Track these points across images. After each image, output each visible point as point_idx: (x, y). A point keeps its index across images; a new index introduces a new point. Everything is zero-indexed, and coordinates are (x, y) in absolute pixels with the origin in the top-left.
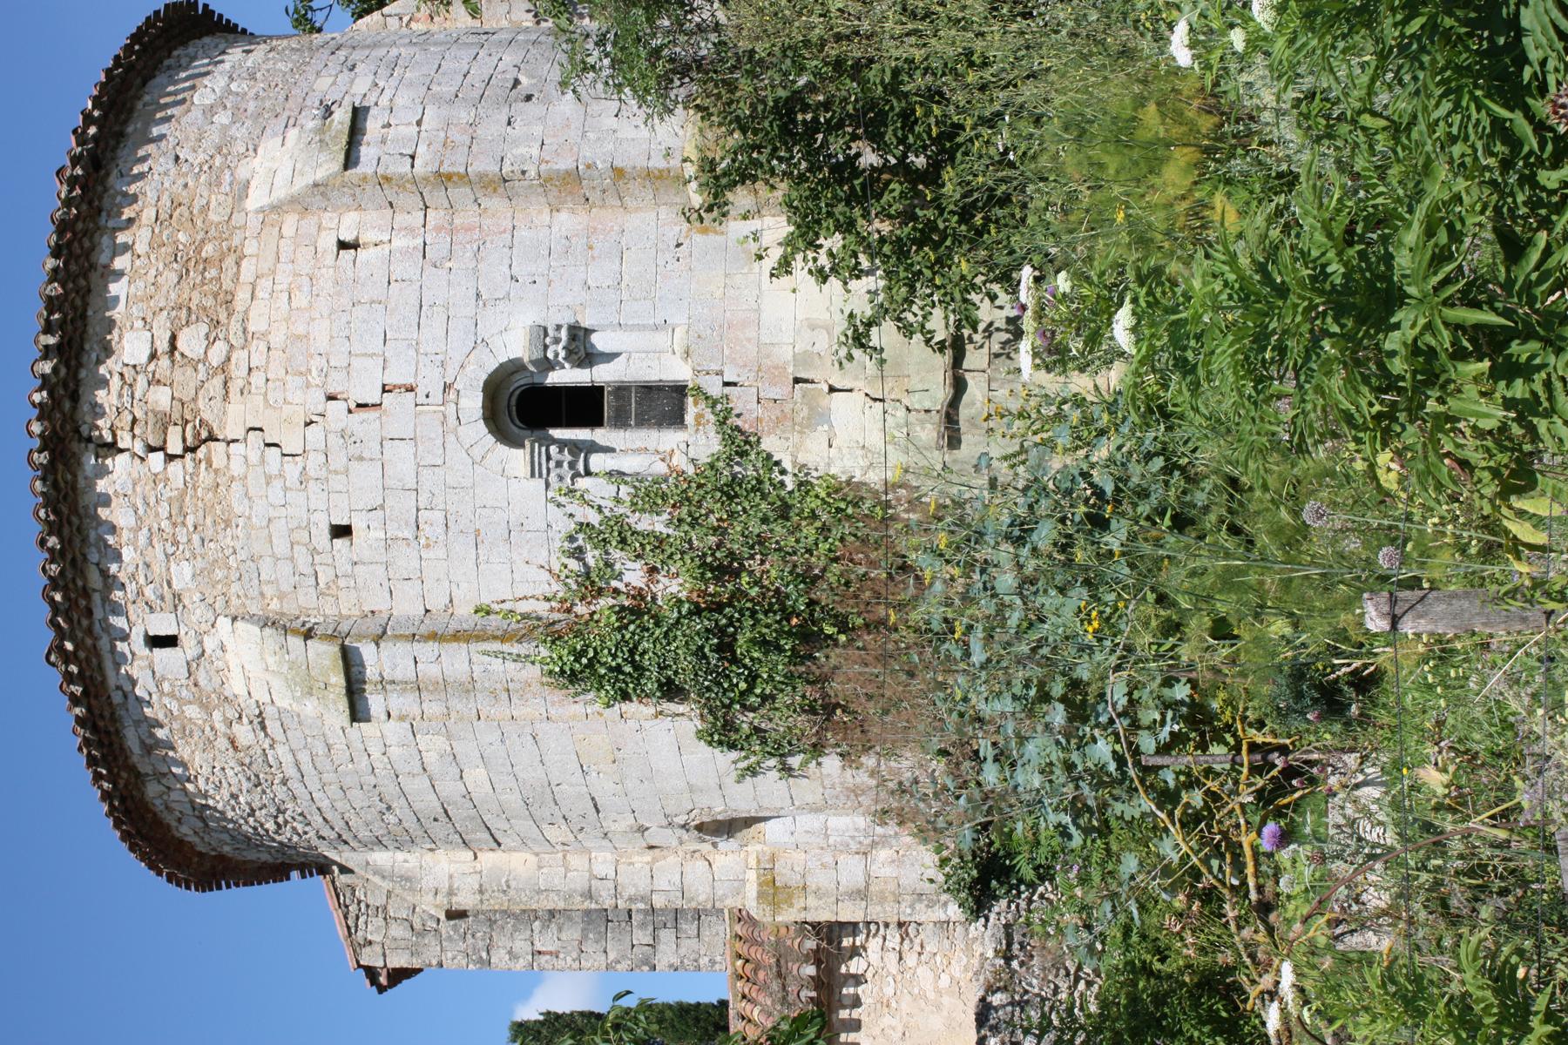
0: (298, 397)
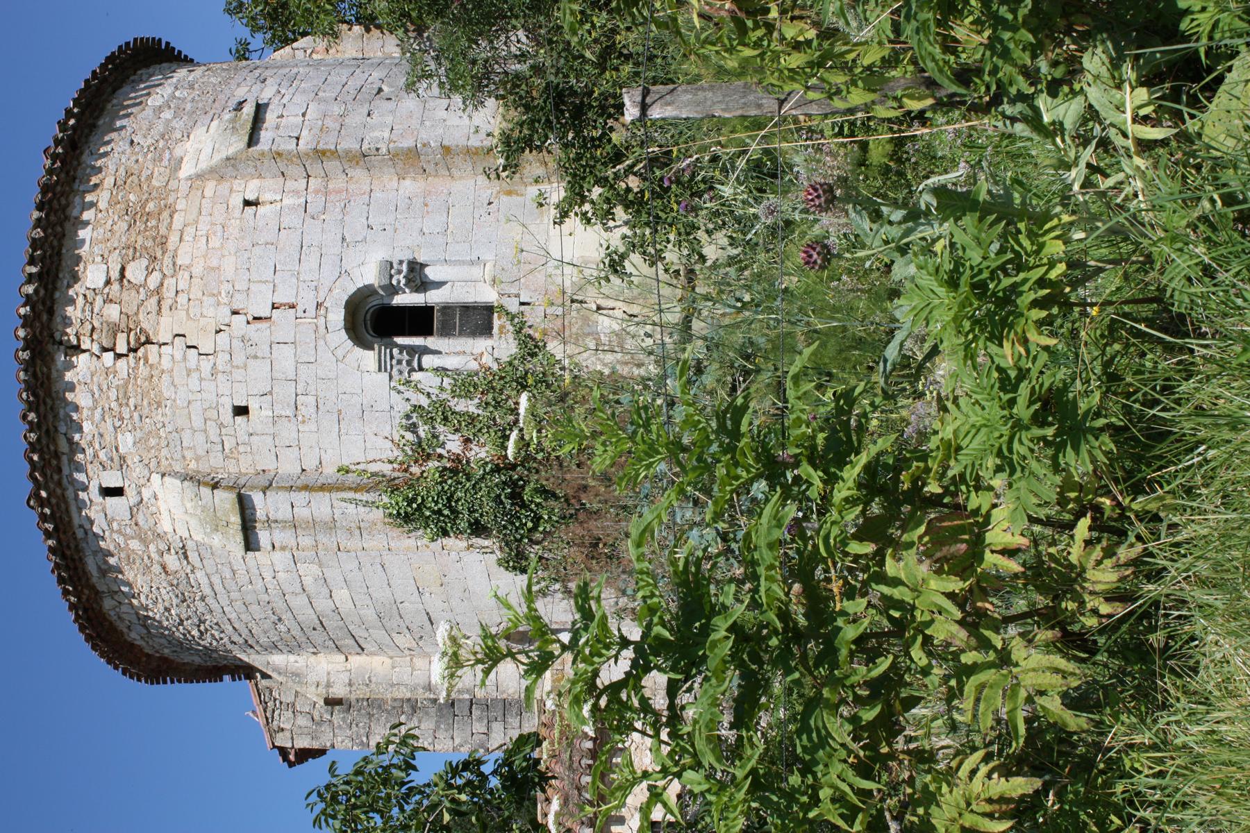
0: (210, 312)
